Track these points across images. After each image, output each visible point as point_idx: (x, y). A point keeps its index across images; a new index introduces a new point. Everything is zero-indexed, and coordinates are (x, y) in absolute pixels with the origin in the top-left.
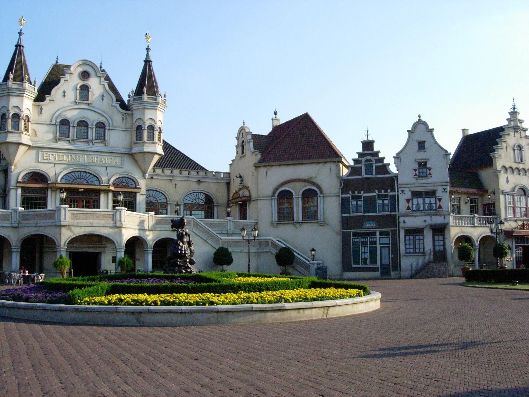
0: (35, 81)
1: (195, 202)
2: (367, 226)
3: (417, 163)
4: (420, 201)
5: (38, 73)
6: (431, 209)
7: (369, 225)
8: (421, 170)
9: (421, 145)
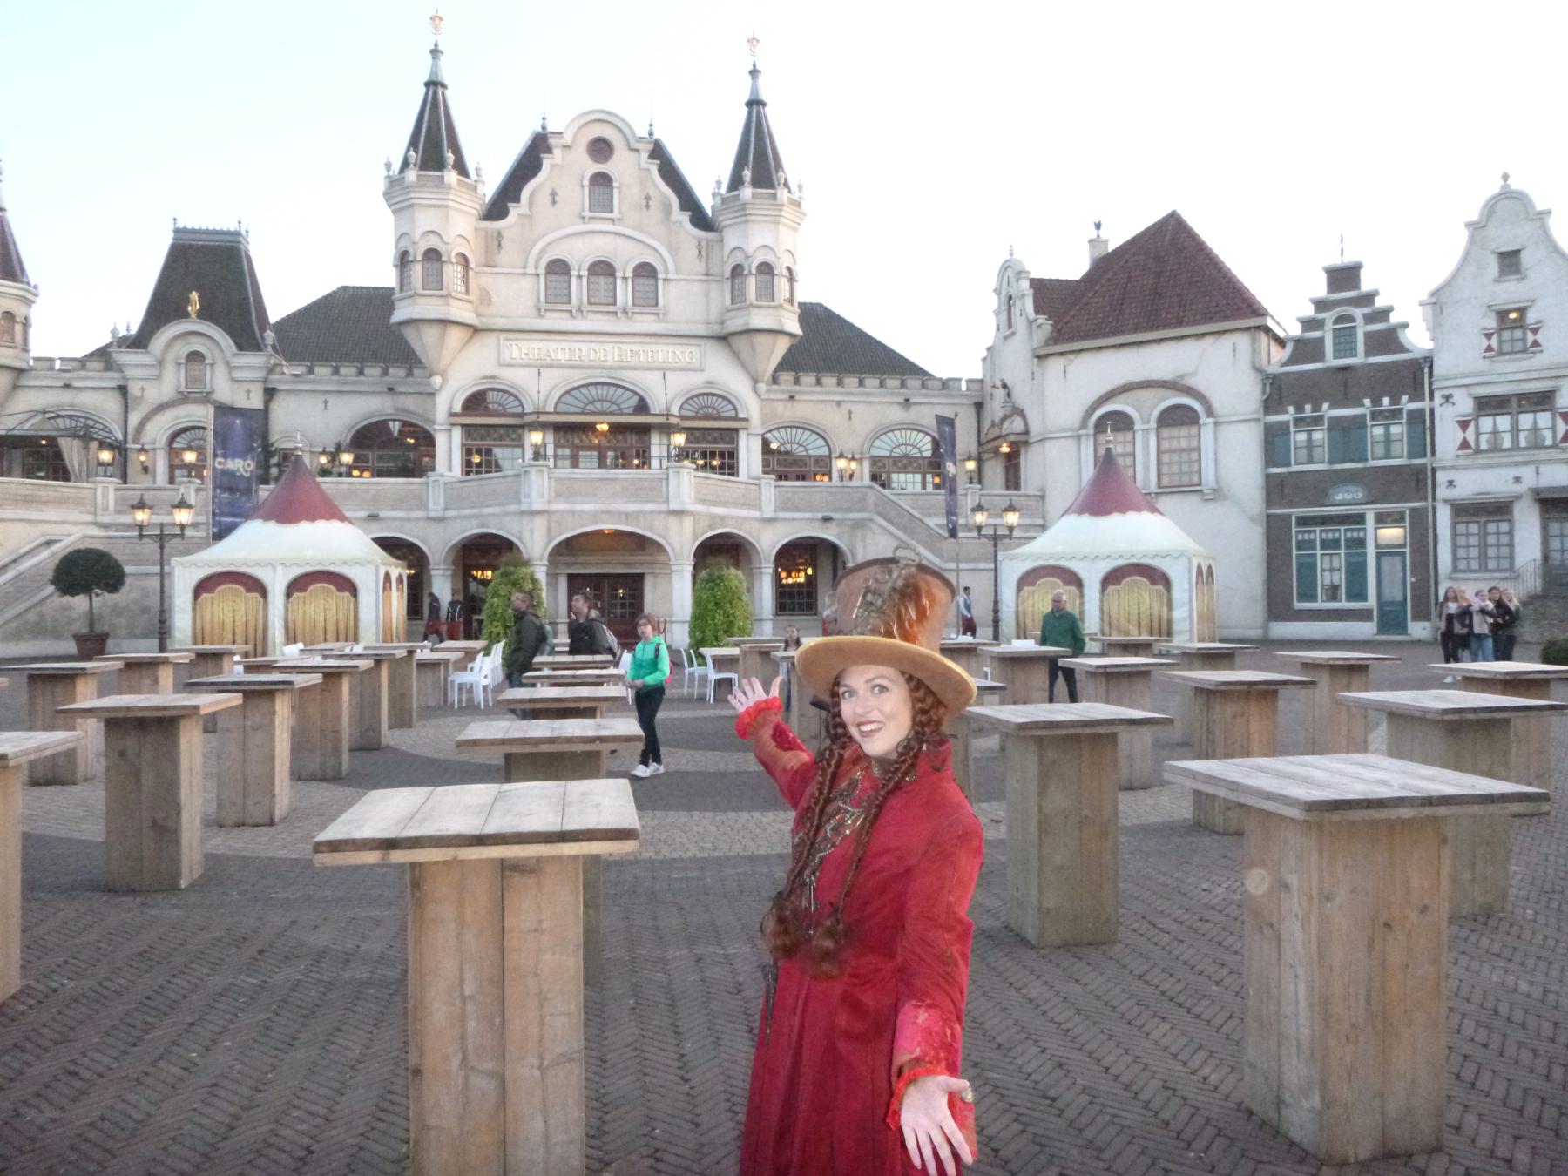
0: (477, 169)
1: (897, 452)
2: (1339, 497)
3: (1493, 315)
4: (1504, 422)
5: (489, 154)
6: (1537, 445)
7: (1345, 498)
8: (1506, 335)
9: (1510, 261)
